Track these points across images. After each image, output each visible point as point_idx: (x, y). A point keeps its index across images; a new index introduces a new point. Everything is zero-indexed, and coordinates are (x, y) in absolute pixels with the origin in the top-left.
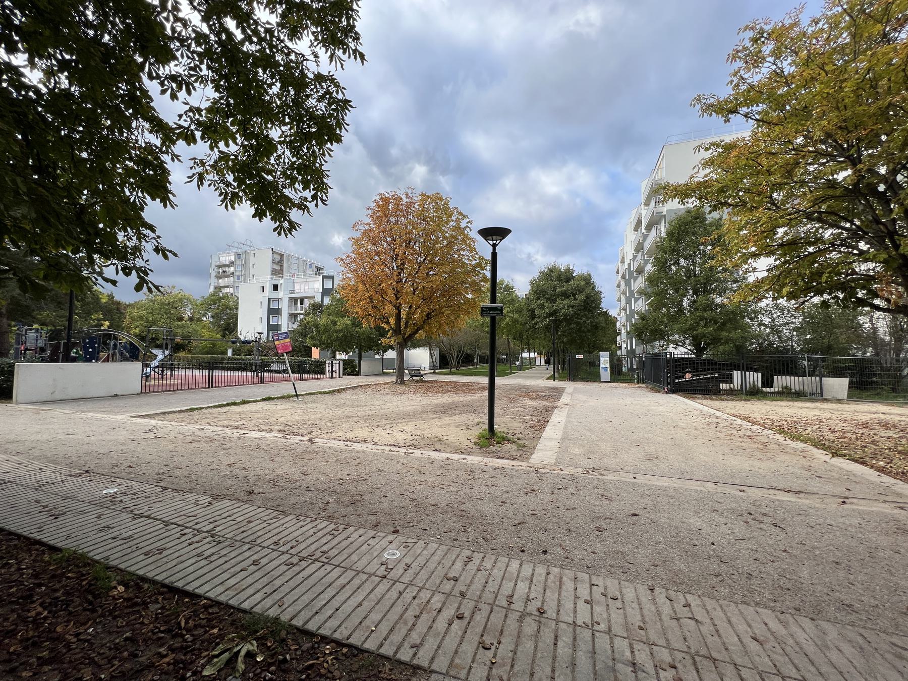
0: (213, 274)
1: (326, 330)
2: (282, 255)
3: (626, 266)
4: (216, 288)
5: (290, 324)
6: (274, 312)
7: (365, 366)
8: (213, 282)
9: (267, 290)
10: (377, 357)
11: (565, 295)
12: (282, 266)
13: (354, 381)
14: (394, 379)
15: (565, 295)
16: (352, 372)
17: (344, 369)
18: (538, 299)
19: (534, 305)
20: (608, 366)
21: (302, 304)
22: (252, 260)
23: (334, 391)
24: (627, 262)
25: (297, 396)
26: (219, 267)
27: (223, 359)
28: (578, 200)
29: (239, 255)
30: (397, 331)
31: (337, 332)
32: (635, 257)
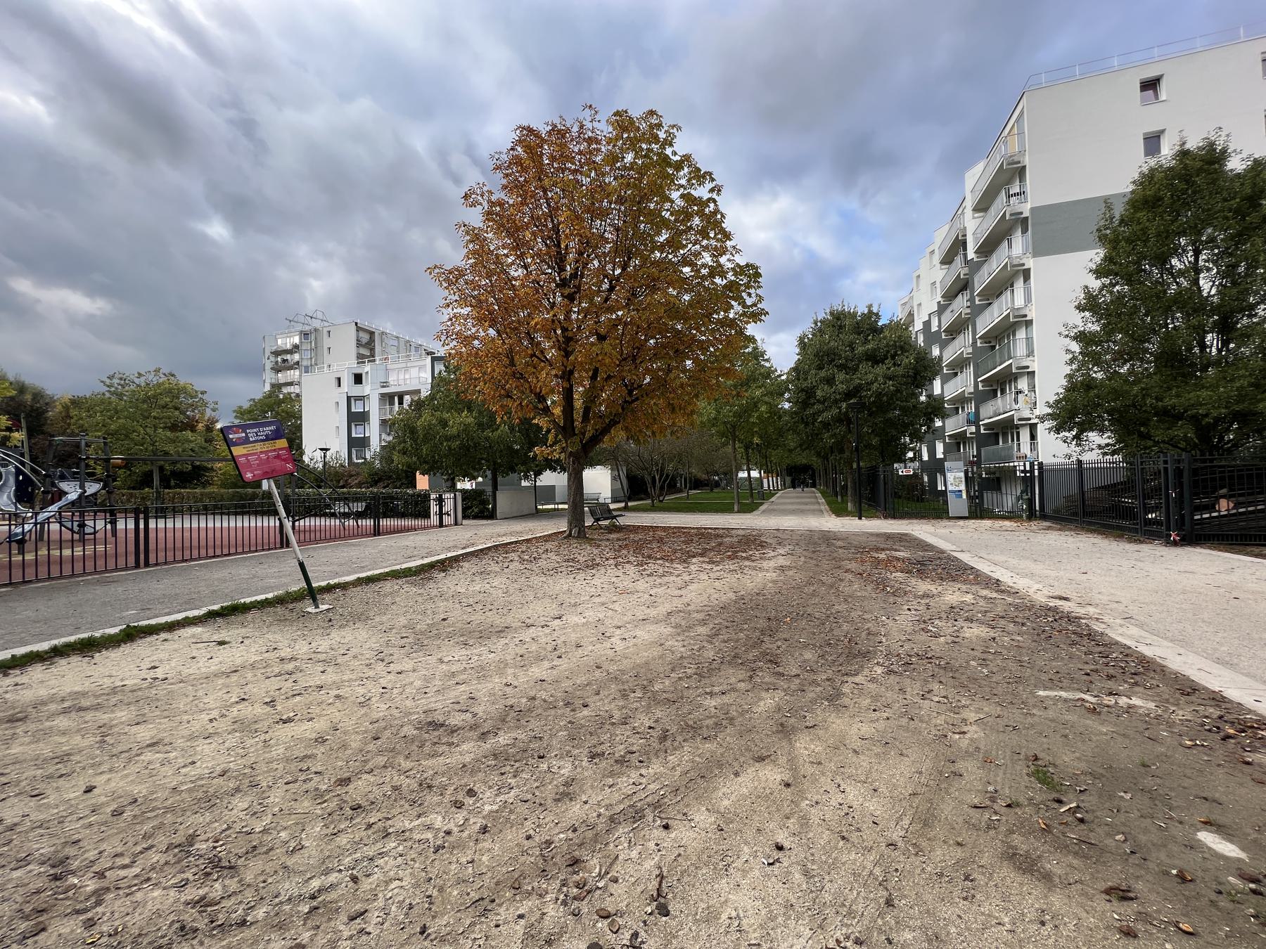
0: (268, 365)
1: (428, 437)
2: (372, 333)
4: (273, 386)
5: (384, 436)
6: (356, 419)
7: (503, 501)
8: (269, 378)
9: (344, 382)
10: (524, 483)
11: (874, 359)
12: (372, 350)
13: (483, 533)
14: (563, 525)
15: (874, 359)
16: (482, 512)
17: (464, 510)
18: (820, 368)
19: (811, 380)
20: (963, 487)
21: (401, 403)
22: (327, 342)
23: (432, 566)
25: (312, 594)
26: (277, 353)
27: (254, 496)
28: (796, 252)
29: (305, 335)
30: (567, 429)
31: (448, 438)
32: (941, 309)
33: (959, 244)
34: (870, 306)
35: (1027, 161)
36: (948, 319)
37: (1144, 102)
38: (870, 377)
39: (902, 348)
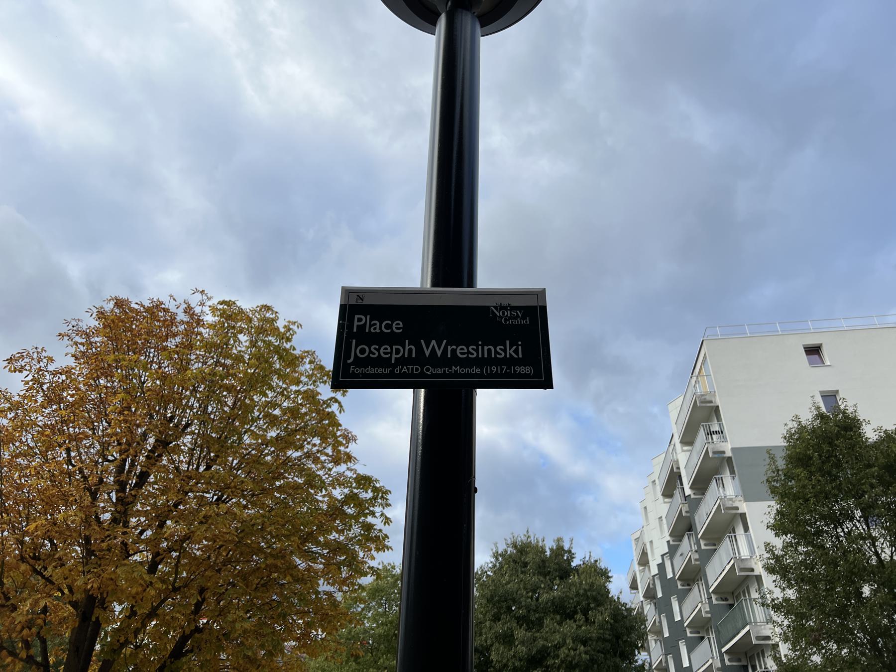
3: (655, 570)
11: (563, 610)
18: (496, 618)
24: (654, 561)
32: (672, 550)
33: (673, 479)
34: (559, 540)
35: (718, 401)
36: (680, 564)
37: (811, 363)
38: (557, 638)
39: (595, 599)
